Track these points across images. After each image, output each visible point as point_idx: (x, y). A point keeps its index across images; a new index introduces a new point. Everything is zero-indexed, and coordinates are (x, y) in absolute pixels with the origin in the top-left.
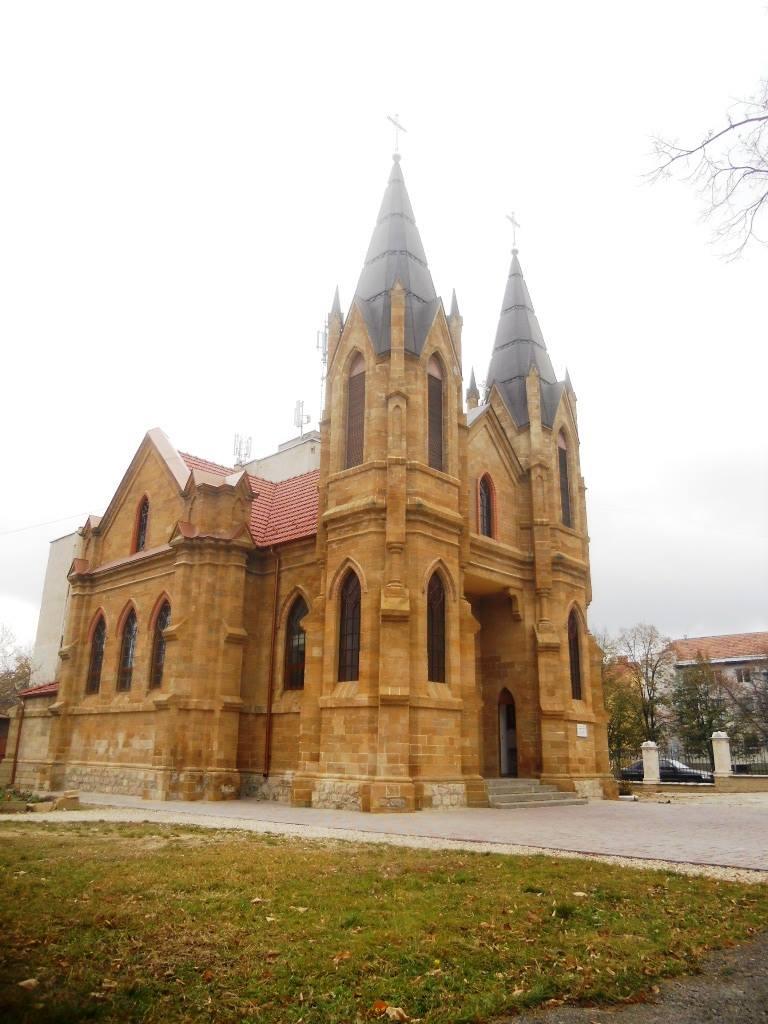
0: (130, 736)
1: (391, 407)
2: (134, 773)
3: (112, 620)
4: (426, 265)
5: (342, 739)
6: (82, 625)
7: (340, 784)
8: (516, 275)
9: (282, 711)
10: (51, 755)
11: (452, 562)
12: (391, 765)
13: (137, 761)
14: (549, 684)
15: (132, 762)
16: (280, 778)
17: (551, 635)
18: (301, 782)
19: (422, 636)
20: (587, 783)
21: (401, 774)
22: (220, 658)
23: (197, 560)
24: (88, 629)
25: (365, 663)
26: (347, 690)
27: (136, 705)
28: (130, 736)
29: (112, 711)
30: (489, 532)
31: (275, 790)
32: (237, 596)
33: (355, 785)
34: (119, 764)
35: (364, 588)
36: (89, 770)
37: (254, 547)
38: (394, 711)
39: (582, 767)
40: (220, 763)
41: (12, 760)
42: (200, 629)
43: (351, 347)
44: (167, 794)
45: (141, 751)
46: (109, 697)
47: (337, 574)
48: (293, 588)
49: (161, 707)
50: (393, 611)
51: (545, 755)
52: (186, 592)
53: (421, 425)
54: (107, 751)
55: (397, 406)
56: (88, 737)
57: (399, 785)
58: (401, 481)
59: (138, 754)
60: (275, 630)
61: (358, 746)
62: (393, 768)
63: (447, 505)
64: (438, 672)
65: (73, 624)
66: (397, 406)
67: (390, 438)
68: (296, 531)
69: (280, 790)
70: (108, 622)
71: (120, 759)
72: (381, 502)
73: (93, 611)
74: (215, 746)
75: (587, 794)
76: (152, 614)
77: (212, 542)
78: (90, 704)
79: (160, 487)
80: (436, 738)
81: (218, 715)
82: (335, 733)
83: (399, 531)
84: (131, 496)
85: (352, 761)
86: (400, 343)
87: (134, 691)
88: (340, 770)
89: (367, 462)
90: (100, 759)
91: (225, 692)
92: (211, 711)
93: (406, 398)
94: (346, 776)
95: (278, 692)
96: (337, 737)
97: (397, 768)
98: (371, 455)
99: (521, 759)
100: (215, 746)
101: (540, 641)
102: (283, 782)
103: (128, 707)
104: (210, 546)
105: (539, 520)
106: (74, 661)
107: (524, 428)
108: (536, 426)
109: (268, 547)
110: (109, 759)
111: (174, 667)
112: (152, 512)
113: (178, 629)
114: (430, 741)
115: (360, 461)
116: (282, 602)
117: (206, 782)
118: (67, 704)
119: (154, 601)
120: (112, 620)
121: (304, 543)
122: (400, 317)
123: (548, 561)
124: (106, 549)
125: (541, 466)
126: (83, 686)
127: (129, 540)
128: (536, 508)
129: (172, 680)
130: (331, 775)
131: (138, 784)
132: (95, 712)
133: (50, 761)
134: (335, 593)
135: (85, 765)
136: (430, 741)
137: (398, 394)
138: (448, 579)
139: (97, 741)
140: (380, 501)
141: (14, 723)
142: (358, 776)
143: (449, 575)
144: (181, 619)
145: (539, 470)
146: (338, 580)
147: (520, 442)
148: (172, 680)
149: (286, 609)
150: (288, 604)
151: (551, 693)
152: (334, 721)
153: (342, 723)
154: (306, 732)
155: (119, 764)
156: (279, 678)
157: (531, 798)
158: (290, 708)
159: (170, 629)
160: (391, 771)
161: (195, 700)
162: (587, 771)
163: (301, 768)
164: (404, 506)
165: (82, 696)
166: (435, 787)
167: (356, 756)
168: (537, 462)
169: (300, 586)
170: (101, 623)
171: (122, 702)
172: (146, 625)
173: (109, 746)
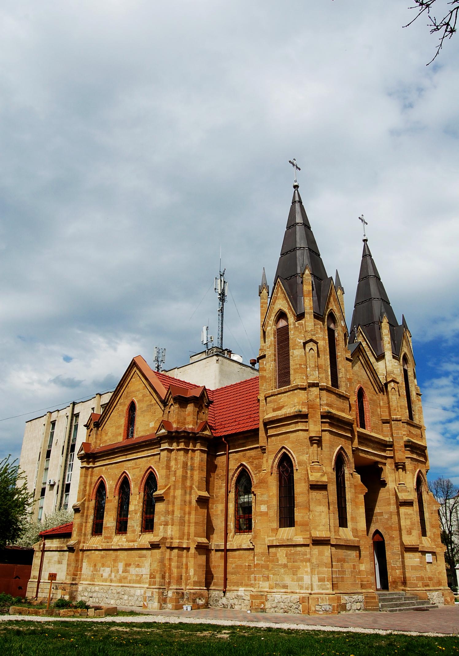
0: (128, 565)
1: (307, 349)
2: (132, 591)
3: (111, 485)
4: (319, 255)
5: (285, 566)
6: (88, 488)
7: (286, 596)
8: (367, 255)
9: (235, 548)
10: (69, 577)
11: (348, 448)
12: (320, 583)
13: (133, 583)
14: (408, 527)
15: (130, 583)
16: (235, 593)
17: (407, 494)
18: (257, 596)
19: (333, 498)
20: (435, 594)
21: (328, 589)
22: (193, 512)
23: (174, 446)
24: (91, 490)
25: (298, 515)
26: (286, 533)
27: (132, 544)
28: (128, 565)
29: (113, 547)
30: (363, 426)
31: (232, 602)
32: (202, 470)
33: (296, 597)
34: (120, 585)
35: (296, 466)
36: (97, 588)
37: (212, 437)
38: (321, 547)
39: (430, 583)
40: (195, 584)
41: (37, 580)
42: (179, 493)
43: (277, 310)
44: (161, 605)
45: (137, 575)
46: (110, 538)
47: (276, 457)
48: (239, 464)
49: (154, 546)
50: (317, 481)
51: (407, 575)
52: (168, 467)
53: (325, 359)
54: (110, 575)
55: (311, 349)
56: (95, 565)
57: (327, 596)
58: (316, 397)
59: (134, 578)
60: (227, 492)
61: (296, 571)
62: (321, 585)
63: (343, 411)
64: (343, 523)
65: (82, 487)
66: (311, 349)
67: (308, 369)
68: (239, 426)
69: (236, 601)
70: (107, 486)
71: (120, 581)
72: (305, 410)
73: (95, 479)
74: (192, 572)
75: (435, 601)
76: (142, 481)
77: (186, 434)
78: (96, 542)
79: (144, 396)
80: (346, 565)
81: (192, 550)
82: (280, 562)
83: (317, 430)
84: (121, 401)
85: (293, 580)
86: (310, 309)
87: (129, 534)
88: (285, 587)
89: (294, 384)
90: (106, 581)
91: (197, 535)
92: (188, 549)
93: (394, 389)
94: (289, 591)
95: (230, 535)
96: (281, 565)
97: (325, 585)
98: (296, 379)
99: (390, 579)
100: (192, 572)
101: (400, 498)
102: (238, 595)
103: (126, 545)
104: (183, 437)
105: (395, 417)
106: (83, 513)
107: (381, 357)
108: (388, 355)
109: (221, 437)
110: (111, 581)
111: (163, 518)
112: (138, 412)
113: (164, 493)
114: (342, 567)
115: (288, 382)
116: (231, 474)
117: (186, 597)
118: (79, 542)
119: (143, 473)
120: (111, 485)
121: (246, 435)
122: (309, 291)
123: (402, 444)
124: (104, 436)
125: (393, 381)
126: (89, 529)
127: (122, 430)
128: (392, 409)
129: (162, 527)
130: (279, 590)
131: (136, 598)
132: (101, 548)
133: (69, 582)
134: (275, 469)
135: (176, 589)
136: (342, 567)
137: (393, 388)
138: (346, 458)
139: (102, 569)
140: (304, 410)
141: (38, 554)
142: (298, 591)
143: (347, 456)
144: (166, 486)
145: (392, 384)
146: (276, 461)
147: (380, 367)
148: (162, 527)
149: (234, 479)
150: (236, 475)
151: (409, 533)
152: (278, 554)
153: (285, 555)
154: (259, 562)
155: (120, 585)
156: (232, 525)
157: (402, 605)
158: (240, 545)
159: (158, 492)
160: (320, 587)
161: (178, 541)
162: (434, 586)
163: (257, 586)
164: (320, 414)
165: (89, 537)
166: (346, 597)
167: (295, 577)
168: (391, 379)
169: (244, 463)
170: (101, 488)
171: (120, 541)
172: (137, 490)
173: (111, 572)
